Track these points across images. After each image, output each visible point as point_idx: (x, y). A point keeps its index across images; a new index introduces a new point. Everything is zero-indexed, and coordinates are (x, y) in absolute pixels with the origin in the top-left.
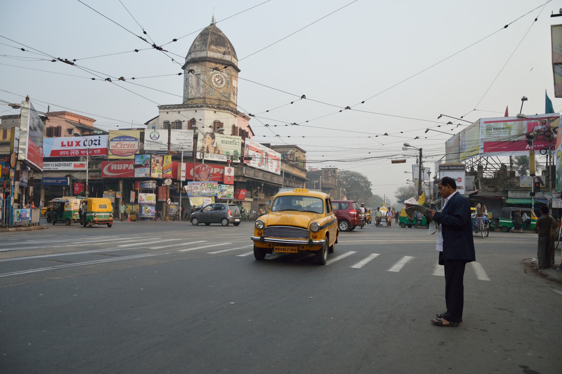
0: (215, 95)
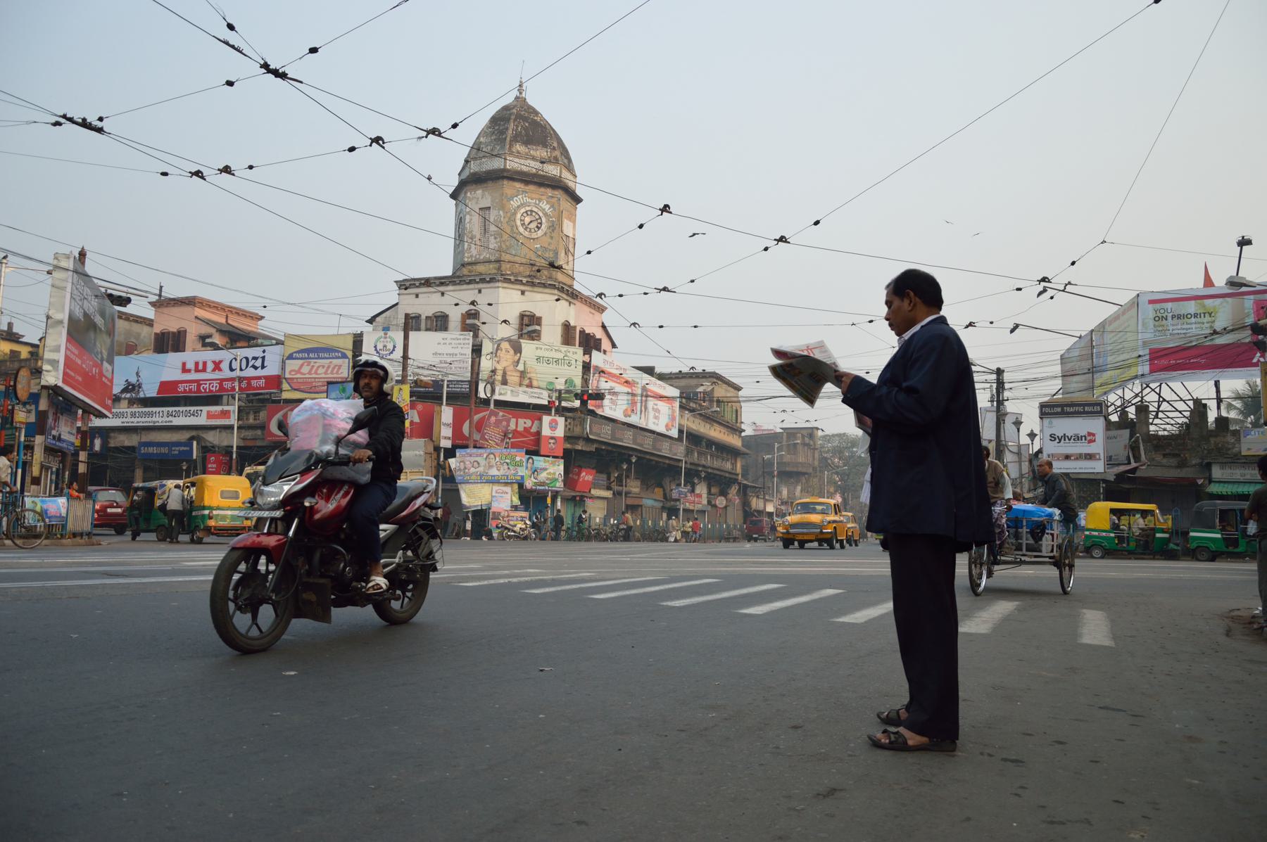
0: (524, 254)
